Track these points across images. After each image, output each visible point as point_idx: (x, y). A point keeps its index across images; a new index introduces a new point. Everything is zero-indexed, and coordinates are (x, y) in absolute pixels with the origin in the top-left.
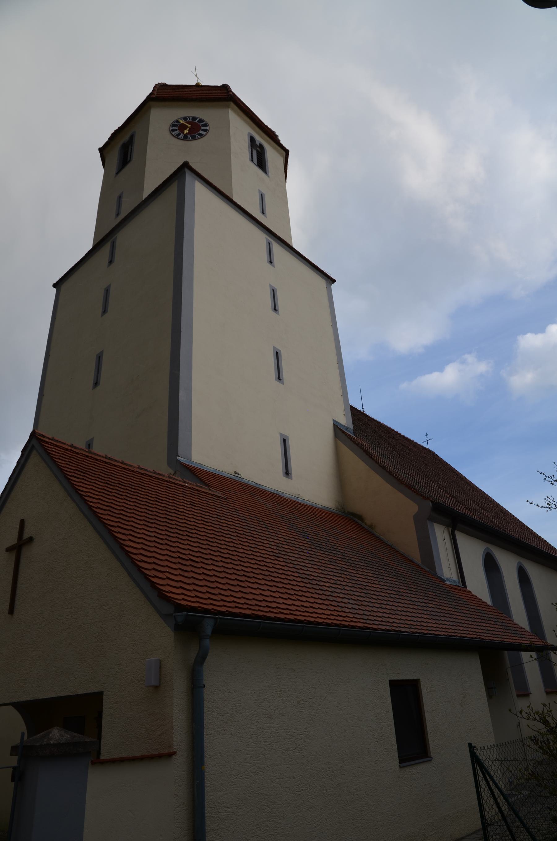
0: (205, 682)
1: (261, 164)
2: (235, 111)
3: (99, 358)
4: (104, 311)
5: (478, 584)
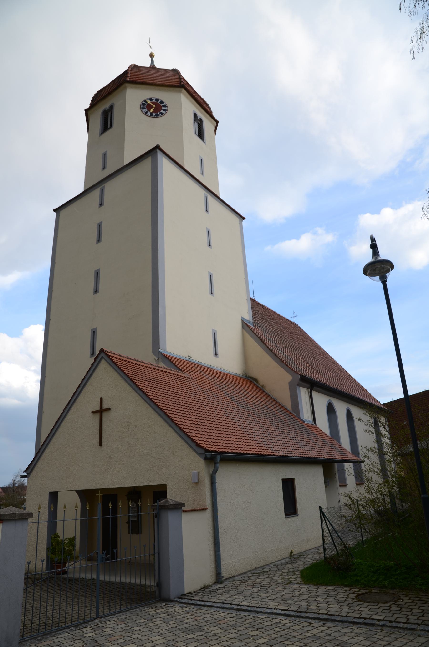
0: (217, 481)
1: (201, 135)
2: (185, 95)
3: (97, 274)
4: (99, 241)
5: (323, 423)
